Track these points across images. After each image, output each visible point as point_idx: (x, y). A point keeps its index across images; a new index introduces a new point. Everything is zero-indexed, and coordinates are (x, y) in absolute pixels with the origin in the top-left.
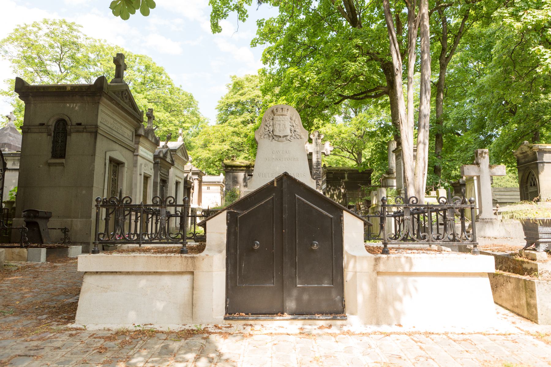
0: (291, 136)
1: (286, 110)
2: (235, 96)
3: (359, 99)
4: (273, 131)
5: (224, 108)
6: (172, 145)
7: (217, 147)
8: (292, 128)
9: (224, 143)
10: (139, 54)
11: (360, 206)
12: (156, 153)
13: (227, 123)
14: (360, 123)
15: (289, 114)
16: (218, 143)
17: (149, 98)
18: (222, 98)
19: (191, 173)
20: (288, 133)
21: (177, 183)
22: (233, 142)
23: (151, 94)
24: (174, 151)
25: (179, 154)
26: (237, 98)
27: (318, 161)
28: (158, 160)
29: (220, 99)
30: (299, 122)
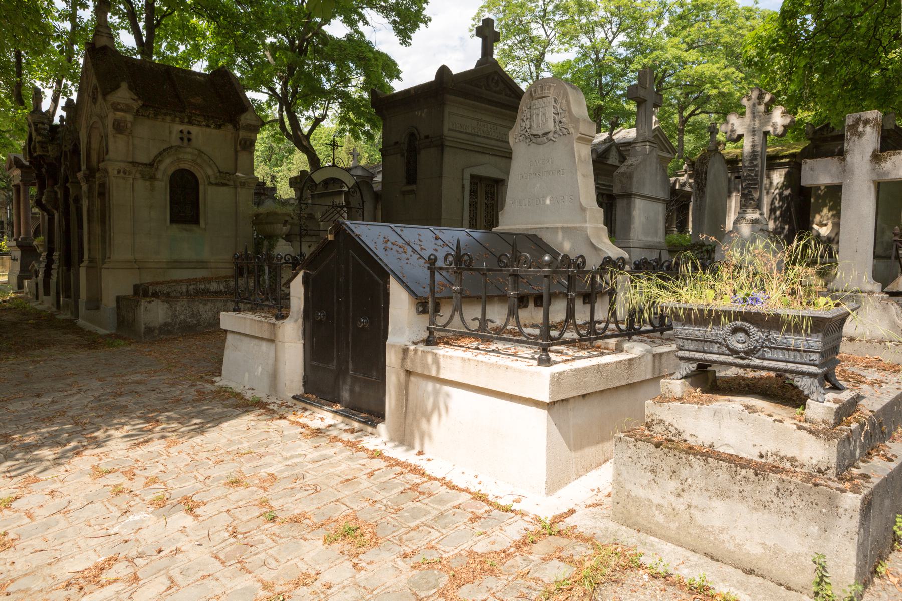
0: (555, 132)
20: (551, 126)
27: (754, 152)
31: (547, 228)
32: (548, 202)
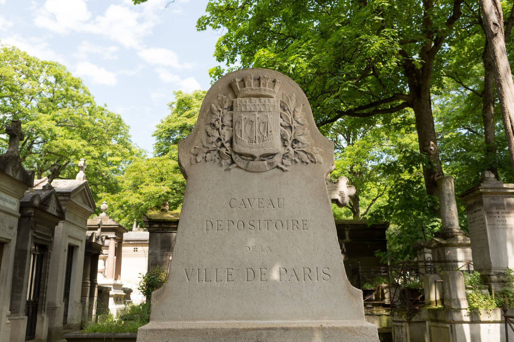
1: (270, 81)
2: (181, 118)
3: (364, 115)
4: (231, 142)
5: (164, 135)
6: (61, 185)
7: (152, 188)
8: (288, 132)
9: (162, 184)
10: (48, 60)
11: (382, 291)
12: (27, 199)
13: (167, 156)
14: (357, 154)
15: (277, 94)
16: (154, 183)
17: (59, 120)
18: (162, 122)
19: (99, 230)
20: (277, 145)
21: (72, 249)
22: (175, 182)
23: (61, 113)
24: (67, 194)
25: (78, 201)
26: (183, 120)
28: (30, 211)
29: (159, 123)
30: (307, 117)
31: (286, 329)
32: (275, 275)
